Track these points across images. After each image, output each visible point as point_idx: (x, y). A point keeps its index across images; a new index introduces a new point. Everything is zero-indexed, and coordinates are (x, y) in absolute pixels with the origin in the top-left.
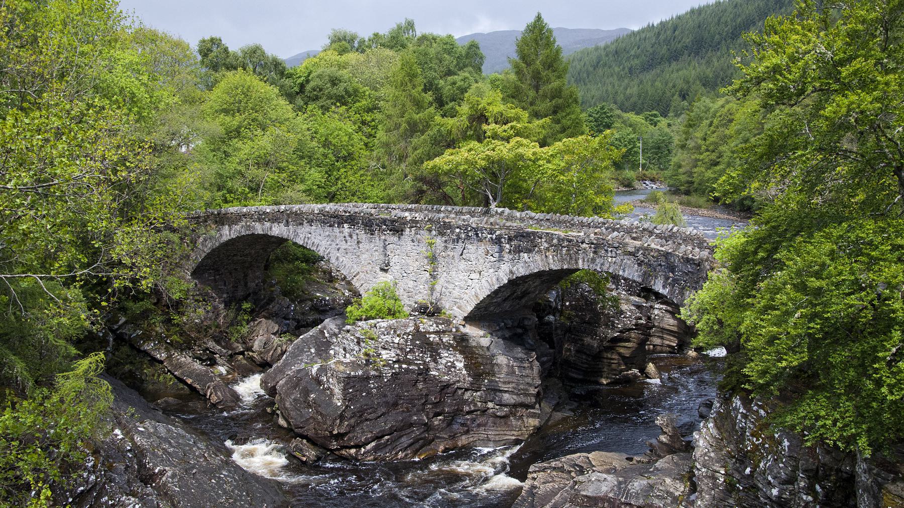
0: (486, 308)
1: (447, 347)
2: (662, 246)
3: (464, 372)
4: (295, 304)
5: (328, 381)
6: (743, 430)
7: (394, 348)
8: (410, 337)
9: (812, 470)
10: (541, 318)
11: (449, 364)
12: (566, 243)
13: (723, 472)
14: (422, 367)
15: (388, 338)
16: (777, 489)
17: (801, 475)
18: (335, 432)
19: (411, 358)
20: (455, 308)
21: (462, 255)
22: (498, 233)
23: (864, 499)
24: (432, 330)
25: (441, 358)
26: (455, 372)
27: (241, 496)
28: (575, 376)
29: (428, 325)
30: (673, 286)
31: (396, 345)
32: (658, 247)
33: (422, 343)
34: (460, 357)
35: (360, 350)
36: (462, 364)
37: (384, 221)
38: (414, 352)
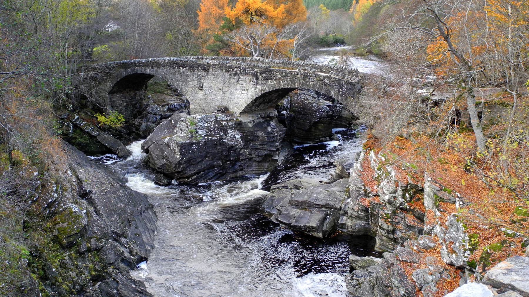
1: (231, 128)
3: (240, 140)
5: (173, 146)
8: (213, 123)
11: (233, 136)
12: (289, 75)
17: (400, 189)
20: (235, 108)
21: (238, 81)
22: (256, 70)
25: (228, 133)
28: (297, 140)
29: (221, 117)
31: (206, 128)
32: (335, 76)
34: (238, 132)
38: (215, 131)
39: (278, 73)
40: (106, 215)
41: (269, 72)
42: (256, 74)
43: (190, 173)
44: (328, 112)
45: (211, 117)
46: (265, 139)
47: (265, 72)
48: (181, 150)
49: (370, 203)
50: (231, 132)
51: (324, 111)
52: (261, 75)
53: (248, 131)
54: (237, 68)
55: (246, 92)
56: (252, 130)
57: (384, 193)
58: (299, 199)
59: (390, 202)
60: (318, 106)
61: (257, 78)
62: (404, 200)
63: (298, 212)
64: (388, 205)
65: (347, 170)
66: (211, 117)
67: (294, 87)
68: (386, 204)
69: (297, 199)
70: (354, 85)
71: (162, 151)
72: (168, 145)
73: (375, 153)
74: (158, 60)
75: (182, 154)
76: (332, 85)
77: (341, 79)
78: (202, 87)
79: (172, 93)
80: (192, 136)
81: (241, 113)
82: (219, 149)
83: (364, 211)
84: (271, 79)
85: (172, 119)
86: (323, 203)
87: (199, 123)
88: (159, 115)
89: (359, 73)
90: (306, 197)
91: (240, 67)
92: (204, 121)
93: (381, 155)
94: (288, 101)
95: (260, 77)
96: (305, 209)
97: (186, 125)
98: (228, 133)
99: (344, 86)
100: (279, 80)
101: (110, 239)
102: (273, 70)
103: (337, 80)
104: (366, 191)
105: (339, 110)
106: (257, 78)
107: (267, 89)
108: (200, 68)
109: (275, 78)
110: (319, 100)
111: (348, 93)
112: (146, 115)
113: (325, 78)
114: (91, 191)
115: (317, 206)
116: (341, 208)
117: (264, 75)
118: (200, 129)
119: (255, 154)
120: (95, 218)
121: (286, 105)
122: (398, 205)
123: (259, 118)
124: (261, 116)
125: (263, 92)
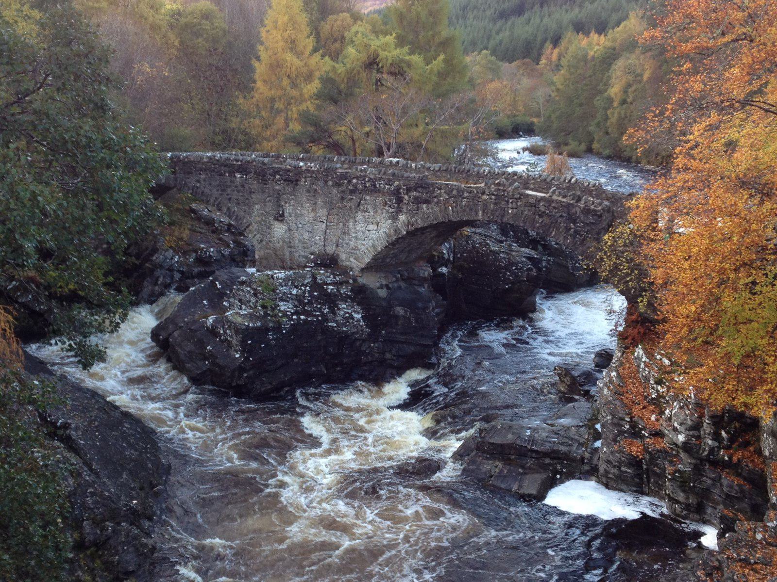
0: (384, 258)
1: (345, 299)
2: (565, 197)
3: (362, 323)
4: (178, 255)
5: (225, 332)
6: (647, 379)
7: (292, 299)
8: (308, 288)
9: (717, 416)
10: (434, 269)
11: (347, 315)
12: (466, 195)
13: (628, 420)
14: (320, 318)
15: (284, 289)
16: (683, 435)
17: (707, 421)
18: (234, 384)
19: (309, 309)
20: (352, 259)
21: (359, 205)
22: (397, 183)
23: (769, 444)
24: (329, 282)
25: (339, 309)
26: (353, 323)
27: (146, 448)
30: (575, 237)
31: (294, 297)
32: (560, 198)
33: (320, 294)
35: (257, 302)
36: (359, 316)
37: (277, 172)
38: (312, 304)
39: (443, 191)
40: (106, 472)
41: (425, 188)
42: (397, 193)
43: (263, 389)
44: (529, 270)
45: (304, 277)
46: (411, 322)
47: (415, 189)
48: (243, 342)
49: (646, 449)
50: (345, 306)
51: (522, 268)
52: (407, 194)
53: (377, 306)
54: (357, 178)
55: (376, 228)
56: (384, 304)
57: (675, 429)
58: (497, 440)
59: (686, 447)
60: (509, 259)
61: (400, 200)
62: (717, 444)
63: (496, 467)
64: (683, 455)
65: (581, 386)
66: (304, 277)
67: (475, 218)
68: (678, 452)
69: (492, 441)
70: (600, 216)
71: (202, 344)
72: (213, 332)
73: (645, 350)
74: (187, 157)
75: (245, 349)
76: (554, 216)
77: (572, 204)
78: (282, 215)
79: (202, 226)
80: (266, 314)
81: (362, 270)
82: (319, 341)
83: (633, 466)
84: (427, 202)
85: (216, 279)
86: (547, 447)
87: (281, 288)
88: (179, 271)
89: (604, 192)
90: (510, 436)
91: (365, 176)
92: (290, 284)
93: (659, 353)
94: (450, 248)
95: (406, 197)
96: (510, 459)
97: (252, 292)
98: (339, 309)
99: (579, 217)
100: (444, 204)
101: (124, 521)
102: (432, 185)
103: (564, 206)
104: (633, 425)
105: (545, 267)
106: (400, 200)
107: (419, 221)
108: (278, 177)
109: (436, 200)
110: (510, 245)
111: (587, 232)
112: (152, 271)
113: (539, 201)
114: (67, 423)
115: (534, 455)
116: (583, 458)
117: (414, 194)
118: (282, 300)
119: (390, 351)
120: (87, 478)
121: (446, 256)
122: (706, 453)
123: (397, 280)
124: (401, 276)
125: (411, 228)
